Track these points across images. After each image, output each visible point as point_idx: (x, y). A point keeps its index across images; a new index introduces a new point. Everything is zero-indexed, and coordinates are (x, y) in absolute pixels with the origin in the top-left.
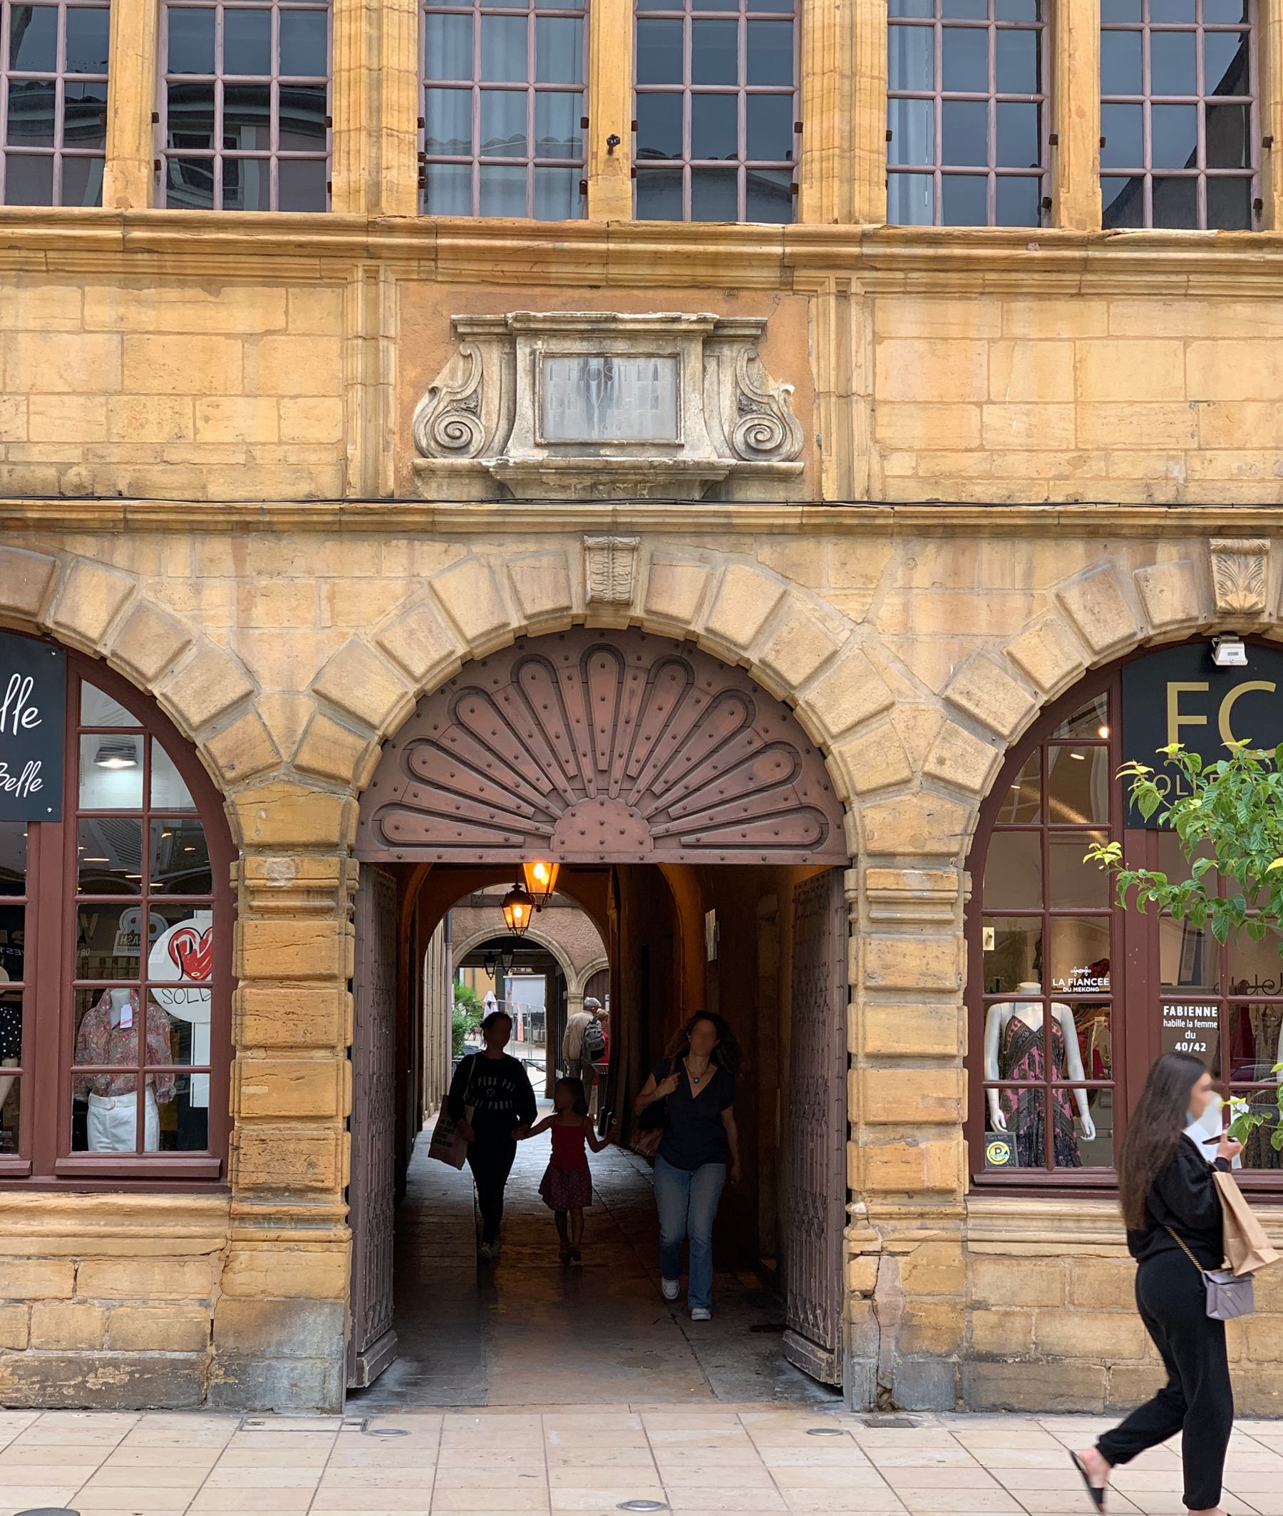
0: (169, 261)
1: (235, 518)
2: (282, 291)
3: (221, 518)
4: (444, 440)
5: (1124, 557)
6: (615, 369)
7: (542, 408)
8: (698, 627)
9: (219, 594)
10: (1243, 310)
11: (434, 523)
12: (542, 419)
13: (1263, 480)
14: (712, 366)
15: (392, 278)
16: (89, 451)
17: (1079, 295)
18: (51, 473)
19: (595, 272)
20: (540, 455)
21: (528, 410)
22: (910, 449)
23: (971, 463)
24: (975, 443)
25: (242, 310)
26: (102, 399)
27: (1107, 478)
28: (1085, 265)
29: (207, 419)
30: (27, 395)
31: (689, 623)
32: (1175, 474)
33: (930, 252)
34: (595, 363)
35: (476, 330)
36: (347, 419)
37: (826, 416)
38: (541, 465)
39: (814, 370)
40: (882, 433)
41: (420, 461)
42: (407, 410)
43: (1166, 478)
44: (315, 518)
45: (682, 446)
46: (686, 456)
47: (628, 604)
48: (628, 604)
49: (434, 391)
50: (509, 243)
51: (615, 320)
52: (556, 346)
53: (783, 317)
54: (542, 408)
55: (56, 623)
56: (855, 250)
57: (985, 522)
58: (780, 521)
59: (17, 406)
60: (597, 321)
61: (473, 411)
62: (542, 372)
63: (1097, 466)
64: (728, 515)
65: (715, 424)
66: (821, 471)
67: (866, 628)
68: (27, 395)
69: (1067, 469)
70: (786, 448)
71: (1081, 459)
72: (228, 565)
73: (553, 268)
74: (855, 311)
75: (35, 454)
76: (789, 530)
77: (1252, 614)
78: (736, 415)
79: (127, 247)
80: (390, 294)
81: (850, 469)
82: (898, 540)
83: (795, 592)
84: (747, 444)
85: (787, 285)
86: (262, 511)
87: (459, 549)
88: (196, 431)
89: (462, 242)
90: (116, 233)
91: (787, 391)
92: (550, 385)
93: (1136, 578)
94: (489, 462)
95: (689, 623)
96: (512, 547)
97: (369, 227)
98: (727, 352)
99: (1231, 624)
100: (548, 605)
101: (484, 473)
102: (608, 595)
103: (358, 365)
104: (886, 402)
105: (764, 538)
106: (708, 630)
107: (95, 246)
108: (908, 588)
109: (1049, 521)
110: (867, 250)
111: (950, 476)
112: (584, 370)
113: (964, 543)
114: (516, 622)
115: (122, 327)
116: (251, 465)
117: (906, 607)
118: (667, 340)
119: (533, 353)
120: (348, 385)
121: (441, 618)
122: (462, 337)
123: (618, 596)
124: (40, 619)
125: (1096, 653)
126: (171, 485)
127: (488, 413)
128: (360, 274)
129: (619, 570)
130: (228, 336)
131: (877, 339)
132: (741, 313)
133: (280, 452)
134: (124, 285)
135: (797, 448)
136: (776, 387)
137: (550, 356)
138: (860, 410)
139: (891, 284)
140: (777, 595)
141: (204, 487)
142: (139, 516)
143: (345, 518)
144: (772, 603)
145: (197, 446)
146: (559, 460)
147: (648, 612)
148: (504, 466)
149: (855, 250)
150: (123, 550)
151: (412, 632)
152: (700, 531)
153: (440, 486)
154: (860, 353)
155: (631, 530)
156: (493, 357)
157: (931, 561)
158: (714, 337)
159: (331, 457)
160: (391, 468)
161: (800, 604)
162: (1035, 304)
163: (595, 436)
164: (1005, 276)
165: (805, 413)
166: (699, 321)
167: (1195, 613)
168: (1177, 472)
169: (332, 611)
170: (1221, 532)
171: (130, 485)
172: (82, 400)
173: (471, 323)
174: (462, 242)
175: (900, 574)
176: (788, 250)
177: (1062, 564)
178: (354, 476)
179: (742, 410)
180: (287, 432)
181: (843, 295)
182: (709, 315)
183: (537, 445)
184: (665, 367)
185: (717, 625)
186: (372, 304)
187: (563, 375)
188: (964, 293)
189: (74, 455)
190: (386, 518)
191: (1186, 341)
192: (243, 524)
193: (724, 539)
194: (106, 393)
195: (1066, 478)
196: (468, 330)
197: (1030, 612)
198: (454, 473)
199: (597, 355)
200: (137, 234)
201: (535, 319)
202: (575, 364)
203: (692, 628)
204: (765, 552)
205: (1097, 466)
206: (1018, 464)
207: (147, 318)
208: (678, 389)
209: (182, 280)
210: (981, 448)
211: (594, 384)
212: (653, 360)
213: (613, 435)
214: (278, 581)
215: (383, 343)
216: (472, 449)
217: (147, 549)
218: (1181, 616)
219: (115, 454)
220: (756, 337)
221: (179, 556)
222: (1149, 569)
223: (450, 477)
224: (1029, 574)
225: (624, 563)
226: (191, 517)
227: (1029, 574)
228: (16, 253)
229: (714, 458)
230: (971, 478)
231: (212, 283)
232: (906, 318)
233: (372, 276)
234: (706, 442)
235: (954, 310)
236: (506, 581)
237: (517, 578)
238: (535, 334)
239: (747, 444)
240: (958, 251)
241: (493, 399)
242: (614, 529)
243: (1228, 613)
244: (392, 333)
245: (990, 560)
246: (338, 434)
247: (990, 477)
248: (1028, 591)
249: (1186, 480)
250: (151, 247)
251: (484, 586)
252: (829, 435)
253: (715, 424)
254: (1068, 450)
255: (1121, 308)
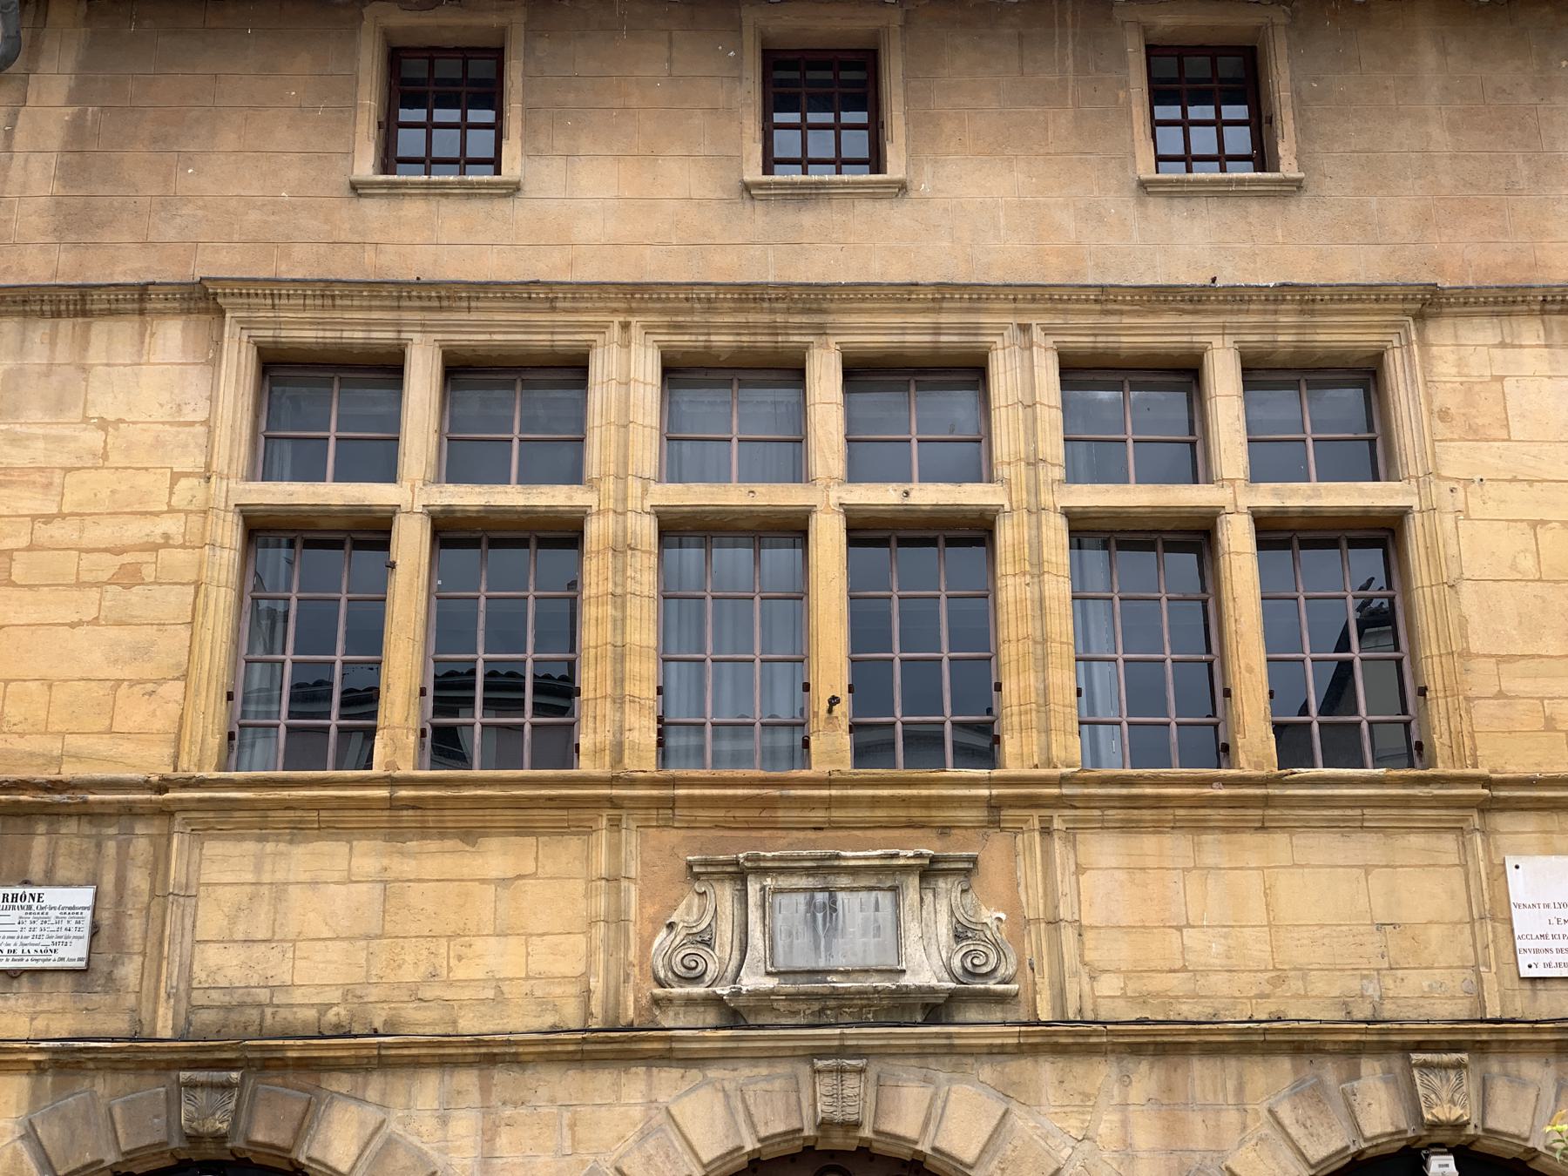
0: (431, 816)
1: (483, 1050)
2: (532, 840)
3: (470, 1051)
4: (680, 970)
5: (1330, 1071)
6: (839, 902)
7: (772, 939)
8: (925, 1147)
9: (465, 1125)
10: (1416, 840)
11: (671, 1050)
12: (772, 949)
13: (1453, 997)
14: (929, 897)
15: (633, 825)
16: (348, 992)
17: (1263, 828)
18: (311, 1014)
19: (819, 815)
20: (770, 983)
21: (759, 942)
22: (1118, 971)
23: (1175, 983)
24: (1178, 965)
25: (496, 857)
26: (363, 943)
27: (1306, 996)
28: (1267, 801)
29: (460, 958)
30: (294, 941)
31: (916, 1143)
32: (1370, 992)
33: (1124, 791)
34: (821, 897)
35: (710, 869)
36: (590, 954)
37: (1036, 941)
38: (772, 992)
39: (1023, 898)
40: (1090, 956)
41: (658, 991)
42: (646, 944)
43: (1362, 996)
44: (559, 1048)
45: (904, 971)
46: (908, 980)
47: (857, 1125)
48: (857, 1125)
49: (671, 926)
50: (740, 792)
51: (838, 857)
52: (784, 882)
53: (992, 852)
54: (772, 939)
55: (309, 1158)
56: (1055, 791)
57: (1194, 1039)
58: (999, 1041)
59: (284, 952)
60: (822, 858)
61: (707, 944)
62: (771, 906)
63: (1296, 985)
64: (949, 1036)
65: (933, 950)
66: (1035, 992)
67: (1087, 1145)
68: (294, 941)
69: (1267, 989)
70: (1001, 972)
71: (1280, 979)
72: (474, 1097)
73: (780, 813)
74: (1058, 845)
75: (298, 997)
76: (1008, 1049)
77: (1458, 1126)
78: (952, 942)
79: (393, 804)
80: (631, 840)
81: (1062, 991)
82: (1112, 1058)
83: (1014, 1106)
84: (965, 969)
85: (995, 823)
86: (509, 1043)
87: (694, 1074)
88: (450, 969)
89: (697, 792)
90: (383, 793)
91: (999, 919)
92: (779, 918)
93: (1344, 1092)
94: (723, 990)
95: (916, 1143)
96: (745, 1071)
97: (613, 781)
98: (942, 884)
99: (1440, 1136)
100: (780, 1128)
101: (718, 1000)
102: (838, 1117)
103: (601, 904)
104: (1092, 927)
105: (984, 1058)
106: (934, 1149)
107: (364, 805)
108: (1124, 1105)
109: (1255, 1038)
110: (1066, 791)
111: (1157, 995)
112: (811, 904)
113: (1176, 1059)
114: (750, 1145)
115: (386, 876)
116: (500, 1000)
117: (1124, 1123)
118: (886, 876)
119: (763, 889)
120: (592, 923)
121: (678, 1144)
122: (697, 877)
123: (847, 1117)
124: (293, 1155)
125: (1312, 1167)
126: (423, 1021)
127: (721, 945)
128: (604, 822)
129: (847, 1092)
130: (483, 881)
131: (1080, 869)
132: (954, 848)
133: (526, 987)
134: (389, 838)
135: (1011, 971)
136: (988, 915)
137: (781, 891)
138: (1068, 935)
139: (1089, 821)
140: (1000, 1113)
141: (455, 1022)
142: (393, 1052)
143: (587, 1047)
144: (995, 1122)
145: (450, 984)
146: (789, 988)
147: (876, 1132)
148: (737, 994)
149: (1055, 791)
150: (375, 1086)
151: (649, 1158)
152: (923, 1053)
153: (677, 1014)
154: (1065, 883)
155: (858, 1053)
156: (725, 894)
157: (1145, 1078)
158: (929, 871)
159: (574, 989)
160: (631, 998)
161: (1022, 1122)
162: (1223, 837)
163: (822, 964)
164: (1194, 812)
165: (1017, 939)
166: (916, 856)
167: (1403, 1126)
168: (1372, 990)
169: (573, 1139)
170: (1419, 1047)
171: (385, 1023)
172: (345, 944)
173: (705, 863)
174: (697, 792)
175: (1116, 1092)
176: (995, 792)
177: (1270, 1080)
178: (596, 1007)
179: (958, 937)
180: (534, 968)
181: (1046, 831)
182: (925, 851)
183: (768, 974)
184: (885, 899)
185: (943, 1145)
186: (614, 849)
187: (792, 908)
188: (1158, 828)
189: (334, 996)
190: (626, 1046)
191: (1367, 869)
192: (491, 1056)
193: (947, 1059)
194: (368, 937)
195: (1268, 996)
196: (703, 870)
197: (1244, 1128)
198: (690, 1001)
199: (822, 890)
200: (403, 793)
201: (765, 859)
202: (801, 898)
203: (919, 1147)
204: (987, 1072)
205: (1296, 985)
206: (1219, 984)
207: (408, 867)
208: (898, 919)
209: (442, 833)
210: (1184, 969)
211: (820, 916)
212: (874, 893)
213: (840, 962)
214: (522, 1111)
215: (624, 883)
216: (707, 978)
217: (398, 1083)
218: (1390, 1129)
219: (374, 994)
220: (968, 870)
221: (428, 1089)
222: (1356, 1084)
223: (686, 1005)
224: (1240, 1089)
225: (852, 1084)
226: (441, 1051)
227: (1240, 1089)
228: (291, 813)
229: (934, 983)
230: (1177, 997)
231: (469, 836)
232: (1105, 851)
233: (615, 824)
234: (926, 968)
235: (1148, 843)
236: (740, 1107)
237: (751, 1101)
238: (765, 872)
239: (965, 969)
240: (1149, 791)
241: (726, 933)
242: (841, 1052)
243: (1435, 1126)
244: (633, 874)
245: (1201, 1075)
246: (581, 968)
247: (1196, 996)
248: (1241, 1107)
249: (1381, 997)
250: (415, 804)
251: (719, 1109)
252: (1041, 957)
253: (933, 950)
254: (1266, 970)
255: (1301, 840)
